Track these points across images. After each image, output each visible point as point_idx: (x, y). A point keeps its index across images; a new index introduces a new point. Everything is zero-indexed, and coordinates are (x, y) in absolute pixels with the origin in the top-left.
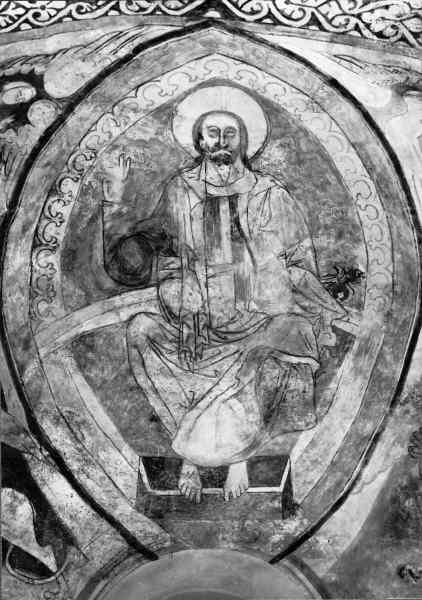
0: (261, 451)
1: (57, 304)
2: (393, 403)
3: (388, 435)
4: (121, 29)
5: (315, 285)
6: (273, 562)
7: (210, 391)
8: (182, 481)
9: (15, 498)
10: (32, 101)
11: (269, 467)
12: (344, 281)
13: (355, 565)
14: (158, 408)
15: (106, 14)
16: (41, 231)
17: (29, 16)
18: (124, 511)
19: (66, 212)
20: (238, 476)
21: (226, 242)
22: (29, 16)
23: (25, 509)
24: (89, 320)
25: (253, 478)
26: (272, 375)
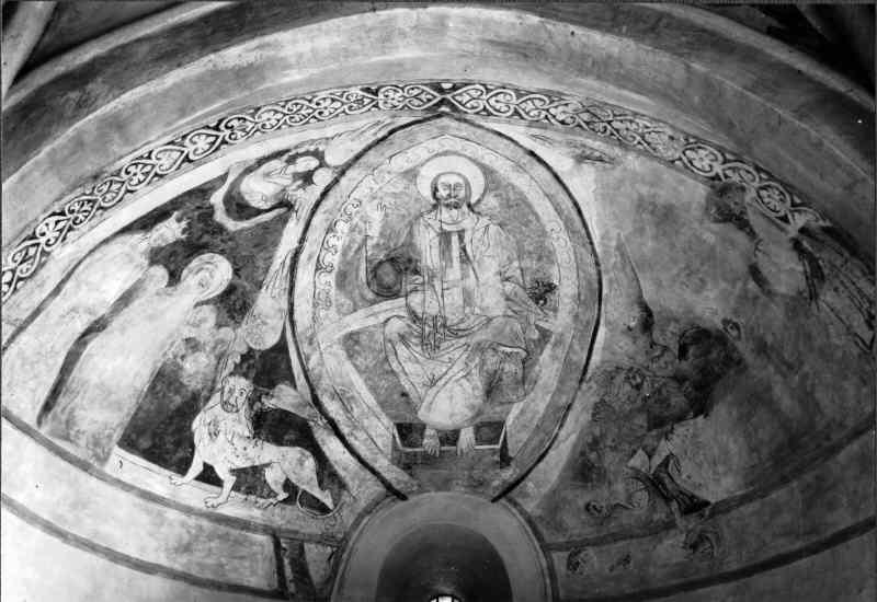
0: (484, 418)
1: (332, 312)
2: (581, 381)
3: (577, 406)
5: (523, 295)
6: (494, 500)
7: (446, 373)
8: (425, 441)
9: (303, 454)
11: (490, 430)
12: (543, 292)
13: (554, 504)
14: (407, 387)
16: (321, 258)
18: (382, 464)
19: (340, 244)
20: (467, 436)
21: (456, 263)
23: (310, 463)
24: (356, 322)
26: (492, 361)
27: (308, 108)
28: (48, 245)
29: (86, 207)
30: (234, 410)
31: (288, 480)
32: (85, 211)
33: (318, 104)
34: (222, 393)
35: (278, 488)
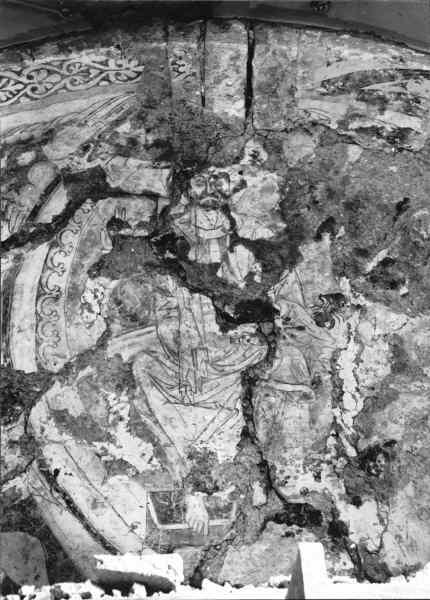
4: (113, 96)
15: (98, 84)
16: (44, 281)
17: (28, 90)
33: (30, 77)
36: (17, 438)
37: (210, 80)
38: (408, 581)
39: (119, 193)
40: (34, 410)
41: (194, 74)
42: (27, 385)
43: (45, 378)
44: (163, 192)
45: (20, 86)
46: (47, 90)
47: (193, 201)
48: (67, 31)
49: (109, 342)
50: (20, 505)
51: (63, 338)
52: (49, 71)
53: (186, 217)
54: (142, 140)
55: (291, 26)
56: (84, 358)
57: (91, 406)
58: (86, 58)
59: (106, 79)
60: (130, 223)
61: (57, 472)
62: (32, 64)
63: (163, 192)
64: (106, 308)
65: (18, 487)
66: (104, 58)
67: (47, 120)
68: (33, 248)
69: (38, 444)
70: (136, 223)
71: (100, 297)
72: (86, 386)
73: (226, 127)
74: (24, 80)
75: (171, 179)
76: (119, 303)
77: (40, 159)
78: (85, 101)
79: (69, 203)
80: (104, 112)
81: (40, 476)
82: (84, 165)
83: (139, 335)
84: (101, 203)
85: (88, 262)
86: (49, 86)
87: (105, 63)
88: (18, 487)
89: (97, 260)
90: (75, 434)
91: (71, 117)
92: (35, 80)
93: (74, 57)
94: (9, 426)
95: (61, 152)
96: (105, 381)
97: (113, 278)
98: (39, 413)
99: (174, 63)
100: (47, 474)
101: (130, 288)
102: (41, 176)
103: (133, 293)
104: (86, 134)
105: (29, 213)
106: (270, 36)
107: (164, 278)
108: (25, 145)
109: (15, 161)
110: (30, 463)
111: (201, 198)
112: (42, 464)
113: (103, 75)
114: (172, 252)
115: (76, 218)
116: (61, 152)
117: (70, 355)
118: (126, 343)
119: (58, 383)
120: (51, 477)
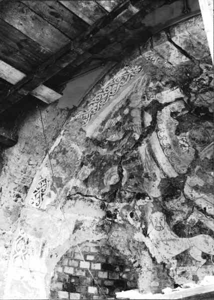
4: (138, 79)
7: (91, 196)
10: (130, 112)
15: (130, 79)
16: (162, 144)
17: (109, 94)
22: (109, 94)
25: (21, 69)
27: (104, 95)
28: (37, 206)
29: (43, 184)
30: (162, 229)
31: (203, 253)
32: (44, 185)
33: (107, 91)
34: (152, 223)
35: (199, 258)
36: (184, 202)
37: (166, 57)
38: (163, 293)
39: (167, 104)
40: (185, 189)
41: (159, 59)
42: (178, 181)
43: (183, 177)
44: (183, 96)
45: (106, 95)
46: (116, 90)
47: (196, 93)
48: (109, 68)
49: (199, 155)
50: (196, 225)
51: (181, 160)
52: (111, 85)
53: (198, 99)
54: (160, 85)
55: (182, 22)
56: (193, 164)
57: (206, 180)
58: (119, 75)
59: (131, 76)
60: (179, 111)
61: (205, 208)
62: (104, 87)
63: (183, 96)
64: (190, 143)
65: (193, 218)
66: (125, 71)
67: (123, 98)
68: (151, 135)
69: (193, 201)
70: (181, 110)
71: (185, 140)
72: (200, 173)
73: (187, 66)
74: (105, 92)
75: (182, 91)
76: (194, 139)
77: (131, 109)
78: (130, 86)
79: (152, 116)
80: (140, 84)
81: (199, 212)
82: (147, 102)
83: (209, 148)
84: (164, 110)
85: (173, 131)
86: (115, 89)
87: (127, 72)
88: (193, 218)
89: (176, 129)
90: (205, 192)
91: (131, 92)
92: (109, 90)
93: (115, 77)
94: (179, 198)
95: (137, 103)
96: (206, 169)
97: (186, 132)
98: (187, 190)
99: (149, 59)
100: (201, 210)
101: (195, 132)
102: (136, 114)
103: (198, 134)
104: (140, 94)
105: (141, 126)
106: (176, 31)
107: (206, 123)
108: (123, 108)
109: (124, 114)
110: (193, 209)
111: (199, 90)
112: (198, 207)
113: (130, 75)
114: (202, 113)
115: (158, 119)
116: (137, 103)
117: (188, 165)
118: (206, 152)
119: (188, 177)
120: (204, 211)
